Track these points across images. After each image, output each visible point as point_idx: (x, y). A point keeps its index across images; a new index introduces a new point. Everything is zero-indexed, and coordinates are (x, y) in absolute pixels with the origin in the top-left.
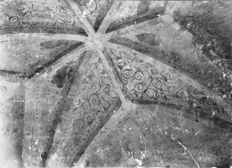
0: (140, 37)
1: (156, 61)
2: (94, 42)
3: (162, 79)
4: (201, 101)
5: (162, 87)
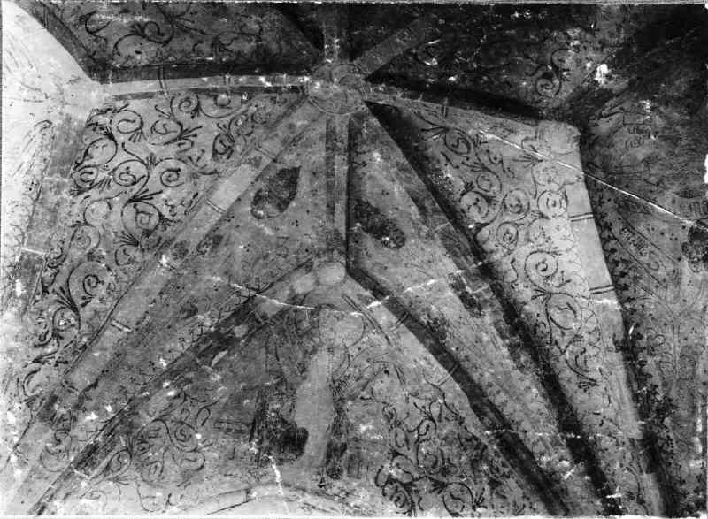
3: (144, 189)
4: (62, 294)
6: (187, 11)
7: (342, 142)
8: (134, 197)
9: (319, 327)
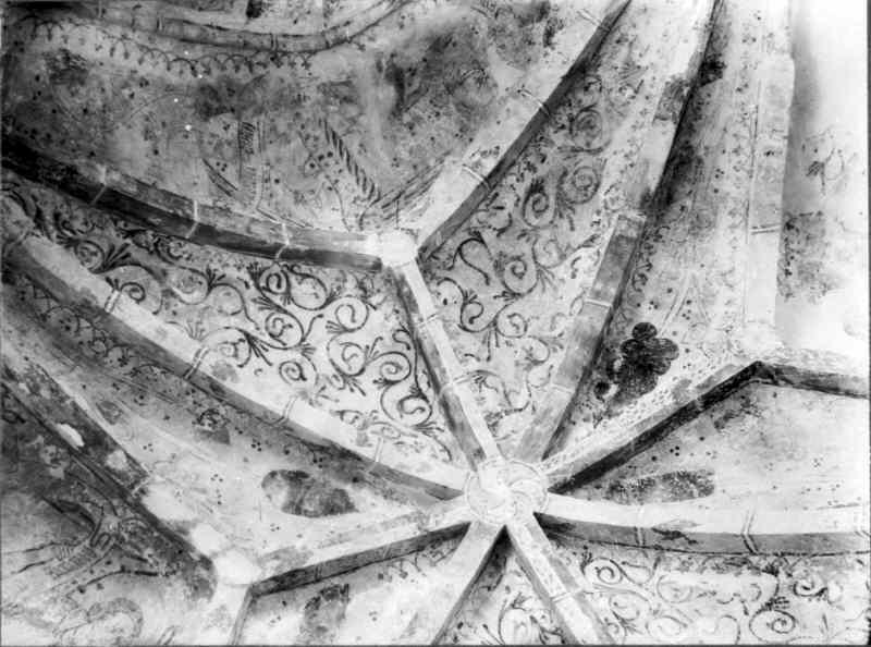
3: (266, 346)
4: (121, 255)
6: (510, 337)
7: (437, 523)
8: (253, 338)
9: (89, 622)
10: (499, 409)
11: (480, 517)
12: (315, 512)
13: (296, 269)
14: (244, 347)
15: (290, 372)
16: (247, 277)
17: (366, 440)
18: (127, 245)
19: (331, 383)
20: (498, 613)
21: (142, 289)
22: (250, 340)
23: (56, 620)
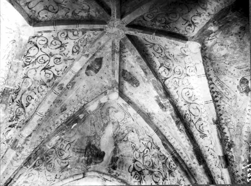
0: (100, 60)
1: (74, 73)
2: (117, 27)
3: (48, 65)
4: (19, 102)
5: (38, 63)
9: (109, 115)
10: (87, 13)
11: (120, 38)
12: (99, 67)
13: (25, 55)
14: (47, 71)
15: (57, 61)
16: (26, 68)
17: (87, 54)
18: (16, 101)
19: (63, 51)
20: (145, 40)
21: (28, 96)
22: (45, 69)
23: (107, 121)
